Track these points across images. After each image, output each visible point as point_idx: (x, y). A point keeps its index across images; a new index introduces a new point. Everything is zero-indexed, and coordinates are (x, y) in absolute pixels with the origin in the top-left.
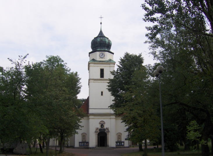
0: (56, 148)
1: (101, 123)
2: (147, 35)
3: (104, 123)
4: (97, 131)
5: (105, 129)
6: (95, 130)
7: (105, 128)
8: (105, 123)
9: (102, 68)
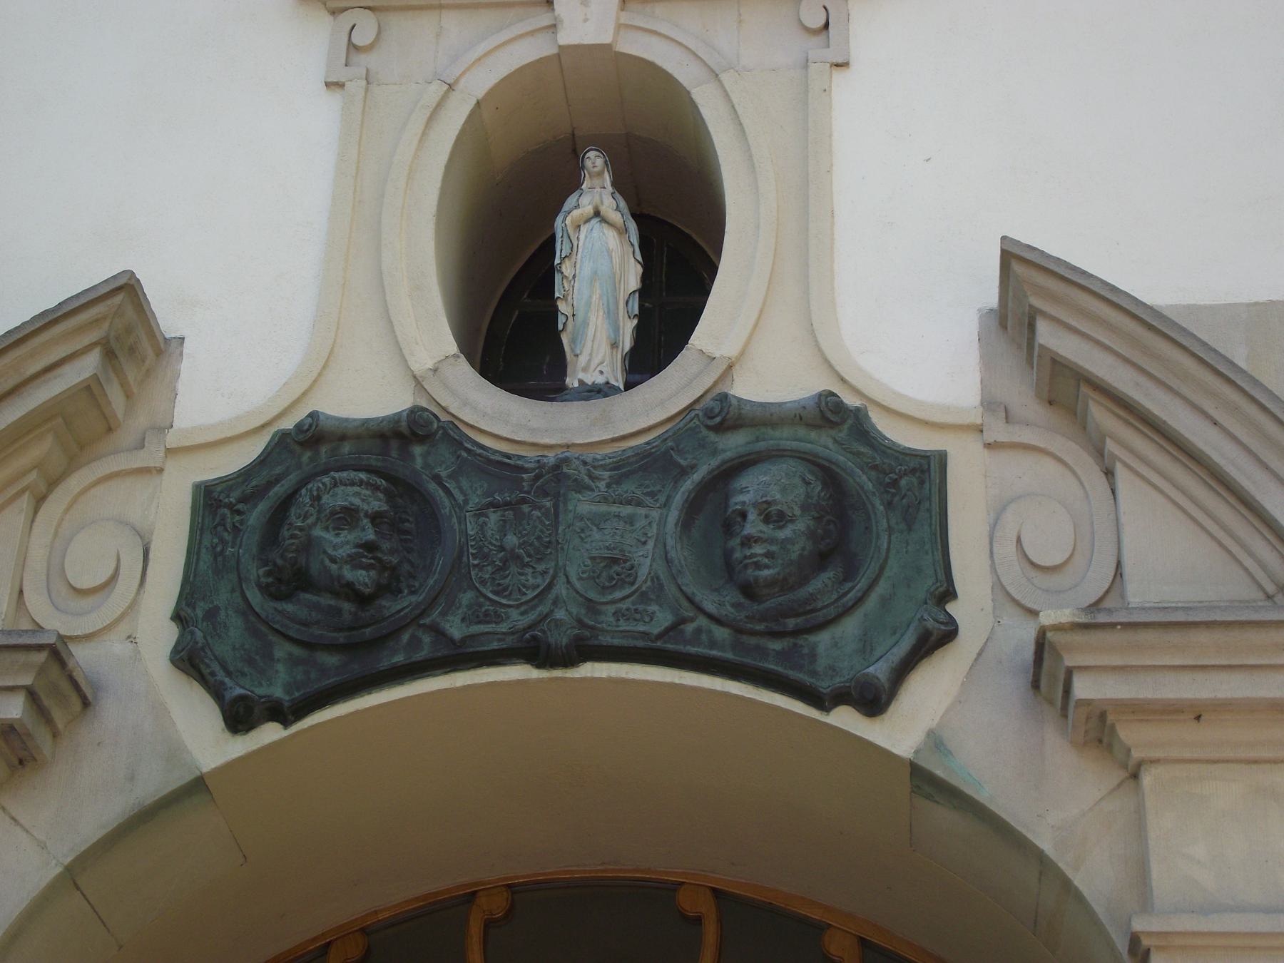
9: (580, 369)
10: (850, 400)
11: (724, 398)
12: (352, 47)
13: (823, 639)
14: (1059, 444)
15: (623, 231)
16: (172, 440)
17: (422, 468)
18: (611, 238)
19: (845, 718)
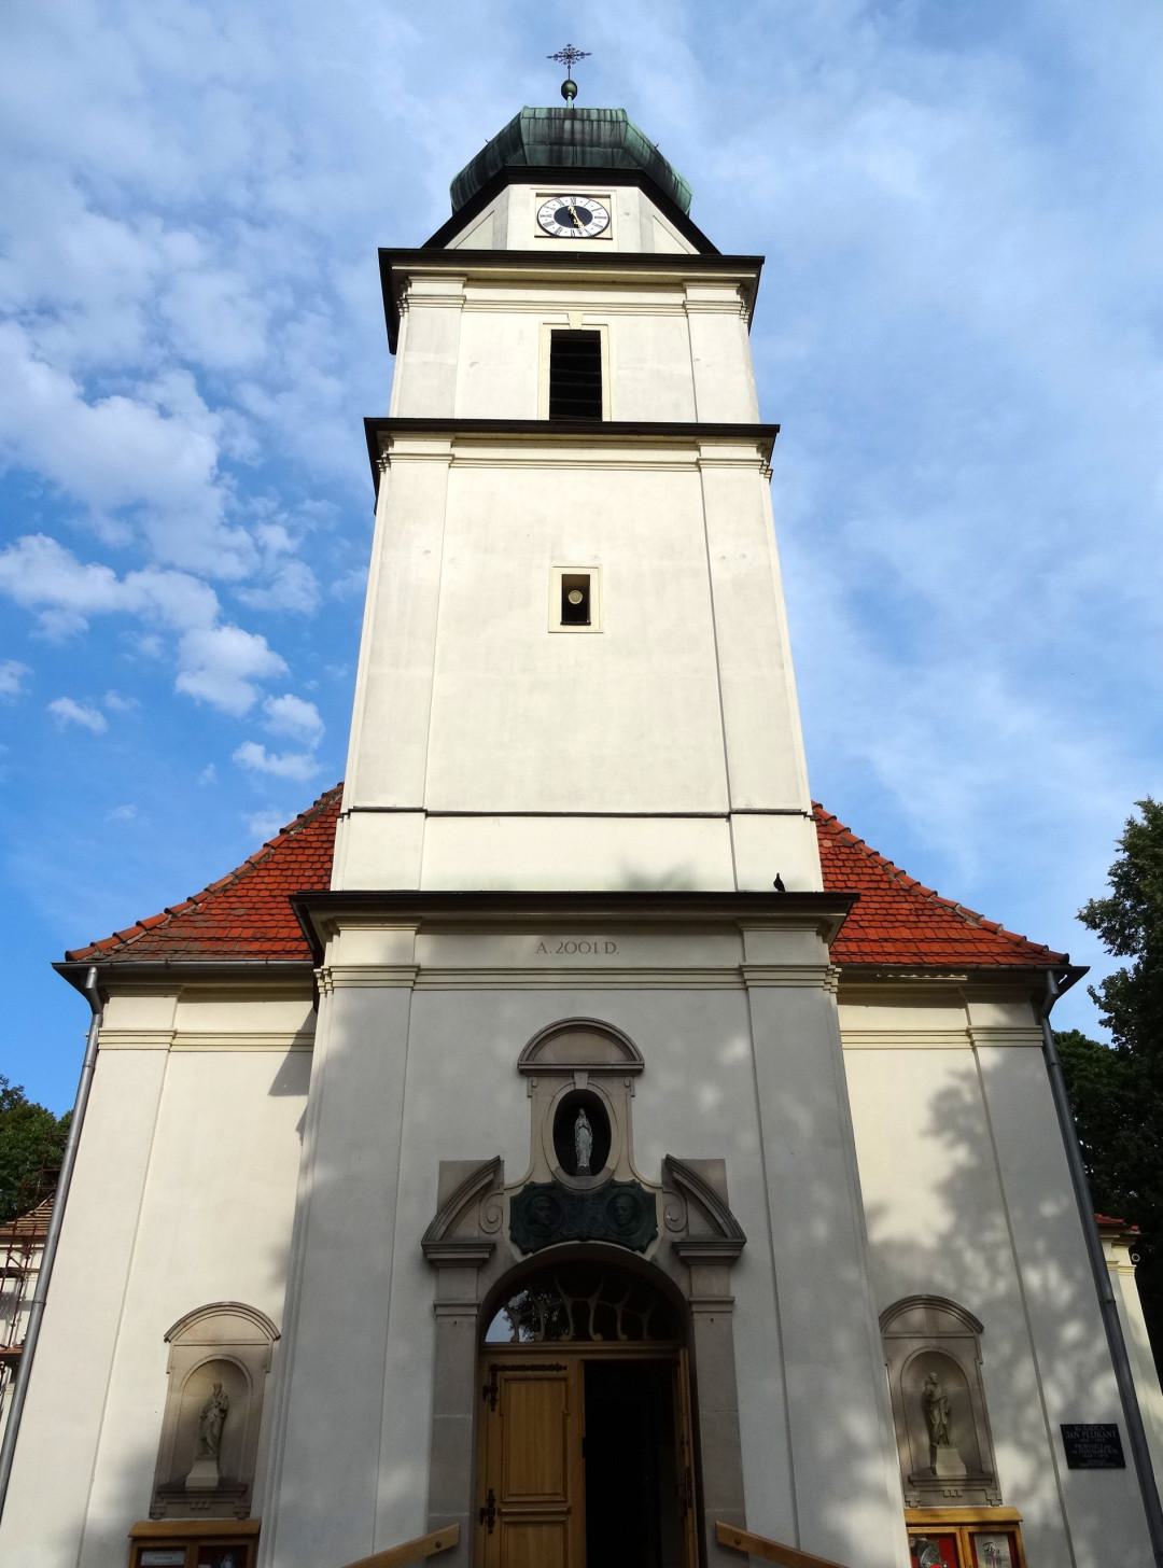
0: (35, 1271)
1: (550, 1055)
2: (1100, 937)
3: (612, 1056)
4: (469, 1229)
5: (633, 1204)
6: (419, 1213)
7: (650, 1174)
8: (632, 1069)
9: (577, 321)
10: (637, 1181)
11: (613, 1180)
12: (533, 1087)
13: (633, 1237)
14: (676, 1193)
15: (588, 1129)
16: (505, 1187)
17: (524, 1253)
18: (586, 1131)
19: (638, 1253)
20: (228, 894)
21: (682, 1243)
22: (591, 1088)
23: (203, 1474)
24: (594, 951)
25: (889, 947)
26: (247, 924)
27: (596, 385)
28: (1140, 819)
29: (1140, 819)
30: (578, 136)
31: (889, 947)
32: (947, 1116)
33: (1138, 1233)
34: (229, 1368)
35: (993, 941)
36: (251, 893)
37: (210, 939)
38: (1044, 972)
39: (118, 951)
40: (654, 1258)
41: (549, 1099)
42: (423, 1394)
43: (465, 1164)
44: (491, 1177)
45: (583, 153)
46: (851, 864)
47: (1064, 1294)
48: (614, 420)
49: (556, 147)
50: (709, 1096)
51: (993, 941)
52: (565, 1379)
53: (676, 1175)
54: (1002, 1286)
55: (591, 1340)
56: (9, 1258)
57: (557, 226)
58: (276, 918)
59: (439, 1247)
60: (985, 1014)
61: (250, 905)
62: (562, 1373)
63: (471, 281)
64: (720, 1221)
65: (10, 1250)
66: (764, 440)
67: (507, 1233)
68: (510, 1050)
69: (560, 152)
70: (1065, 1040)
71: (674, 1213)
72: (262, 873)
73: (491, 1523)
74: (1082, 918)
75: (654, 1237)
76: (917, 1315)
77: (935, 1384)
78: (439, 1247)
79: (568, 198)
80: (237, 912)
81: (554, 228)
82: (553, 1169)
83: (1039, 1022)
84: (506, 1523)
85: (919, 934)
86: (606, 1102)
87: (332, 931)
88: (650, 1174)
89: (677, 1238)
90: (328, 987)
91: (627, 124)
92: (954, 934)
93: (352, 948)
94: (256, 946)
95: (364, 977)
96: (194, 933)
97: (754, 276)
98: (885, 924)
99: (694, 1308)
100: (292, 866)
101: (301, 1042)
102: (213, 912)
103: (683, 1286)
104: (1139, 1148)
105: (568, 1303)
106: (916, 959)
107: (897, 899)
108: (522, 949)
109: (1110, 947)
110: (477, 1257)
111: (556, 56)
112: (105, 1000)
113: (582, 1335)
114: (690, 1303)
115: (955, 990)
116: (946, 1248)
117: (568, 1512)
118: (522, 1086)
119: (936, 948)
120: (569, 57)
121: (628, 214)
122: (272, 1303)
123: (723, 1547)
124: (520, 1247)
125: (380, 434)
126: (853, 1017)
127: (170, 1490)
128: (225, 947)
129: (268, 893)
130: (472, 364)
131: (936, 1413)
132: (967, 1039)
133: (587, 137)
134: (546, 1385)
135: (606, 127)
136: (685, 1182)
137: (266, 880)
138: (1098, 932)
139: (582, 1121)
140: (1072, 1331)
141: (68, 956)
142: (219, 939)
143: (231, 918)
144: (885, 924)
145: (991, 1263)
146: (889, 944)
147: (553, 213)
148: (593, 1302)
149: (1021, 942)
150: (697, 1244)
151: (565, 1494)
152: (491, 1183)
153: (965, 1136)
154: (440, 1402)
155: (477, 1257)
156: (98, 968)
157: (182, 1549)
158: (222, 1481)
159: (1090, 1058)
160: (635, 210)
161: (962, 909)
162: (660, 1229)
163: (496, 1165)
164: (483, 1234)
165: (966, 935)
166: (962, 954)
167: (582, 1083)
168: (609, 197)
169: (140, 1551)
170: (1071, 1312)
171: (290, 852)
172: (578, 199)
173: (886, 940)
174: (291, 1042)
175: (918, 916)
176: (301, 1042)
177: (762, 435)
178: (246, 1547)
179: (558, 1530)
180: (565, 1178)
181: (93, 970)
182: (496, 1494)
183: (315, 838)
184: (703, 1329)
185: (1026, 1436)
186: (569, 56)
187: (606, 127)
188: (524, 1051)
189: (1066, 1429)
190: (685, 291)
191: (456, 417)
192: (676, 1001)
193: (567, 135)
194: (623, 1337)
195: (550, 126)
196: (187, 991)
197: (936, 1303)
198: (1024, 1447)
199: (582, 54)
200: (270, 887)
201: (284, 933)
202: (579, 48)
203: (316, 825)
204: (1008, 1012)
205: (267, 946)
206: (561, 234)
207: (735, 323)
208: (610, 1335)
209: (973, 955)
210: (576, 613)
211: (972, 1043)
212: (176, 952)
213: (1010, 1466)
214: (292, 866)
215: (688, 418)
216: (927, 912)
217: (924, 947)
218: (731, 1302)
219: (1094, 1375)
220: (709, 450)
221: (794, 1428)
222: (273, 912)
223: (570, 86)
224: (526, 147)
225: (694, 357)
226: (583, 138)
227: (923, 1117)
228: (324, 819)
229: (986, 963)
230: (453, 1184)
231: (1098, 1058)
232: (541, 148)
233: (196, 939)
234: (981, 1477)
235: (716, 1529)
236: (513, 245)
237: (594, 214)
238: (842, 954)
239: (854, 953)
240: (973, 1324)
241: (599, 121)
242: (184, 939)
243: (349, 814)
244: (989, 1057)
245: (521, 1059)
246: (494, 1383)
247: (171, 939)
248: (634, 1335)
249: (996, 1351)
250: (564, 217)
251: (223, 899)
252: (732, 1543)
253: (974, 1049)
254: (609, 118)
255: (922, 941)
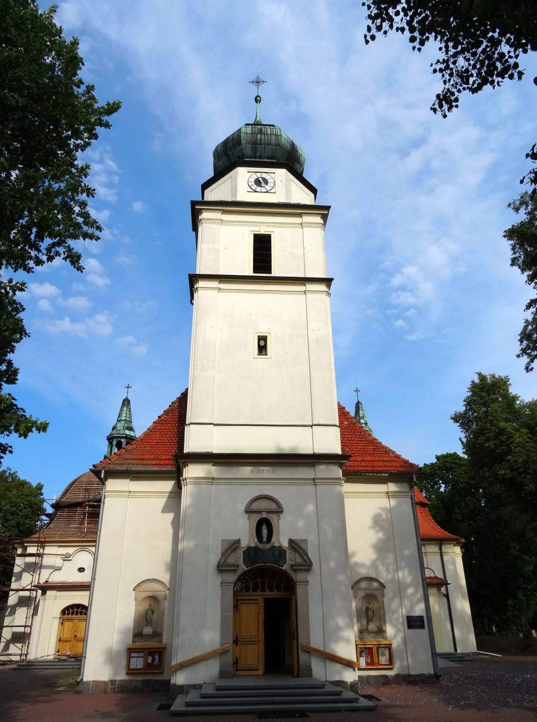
1: (256, 506)
2: (459, 426)
3: (274, 507)
4: (231, 560)
5: (280, 553)
6: (215, 557)
7: (285, 544)
8: (279, 511)
9: (263, 231)
17: (247, 567)
19: (281, 567)
20: (143, 441)
21: (295, 565)
22: (267, 517)
23: (148, 630)
24: (266, 472)
25: (363, 464)
26: (151, 453)
27: (268, 252)
28: (477, 381)
29: (477, 381)
30: (263, 141)
31: (363, 464)
32: (377, 522)
33: (464, 541)
34: (154, 599)
35: (398, 461)
36: (151, 441)
37: (139, 459)
38: (412, 474)
39: (109, 464)
40: (286, 569)
41: (254, 520)
42: (218, 609)
43: (229, 541)
44: (237, 545)
45: (265, 148)
46: (353, 431)
47: (409, 579)
48: (276, 276)
49: (254, 146)
50: (301, 523)
51: (398, 461)
52: (259, 603)
53: (293, 544)
54: (390, 577)
55: (266, 591)
56: (38, 550)
57: (255, 186)
58: (160, 451)
59: (222, 566)
60: (392, 487)
61: (151, 446)
62: (258, 601)
63: (224, 212)
64: (306, 558)
65: (38, 546)
66: (328, 283)
67: (242, 561)
68: (242, 507)
69: (256, 147)
70: (450, 456)
71: (292, 555)
72: (154, 433)
73: (237, 644)
74: (452, 418)
75: (286, 562)
76: (363, 584)
77: (369, 604)
78: (222, 566)
79: (259, 174)
80: (146, 449)
81: (254, 187)
82: (256, 542)
83: (410, 489)
84: (242, 644)
85: (374, 458)
86: (272, 521)
87: (186, 465)
88: (285, 544)
89: (293, 563)
90: (185, 484)
91: (281, 136)
92: (385, 459)
93: (192, 471)
94: (155, 462)
95: (197, 481)
96: (134, 457)
97: (327, 212)
98: (363, 455)
99: (297, 584)
100: (164, 430)
101: (171, 495)
102: (139, 448)
103: (294, 577)
104: (474, 503)
105: (259, 581)
106: (372, 469)
107: (368, 445)
108: (246, 471)
109: (463, 430)
110: (233, 569)
111: (253, 82)
112: (106, 480)
113: (263, 590)
114: (296, 582)
115: (384, 478)
116: (374, 565)
117: (259, 641)
118: (246, 516)
119: (379, 464)
120: (258, 83)
121: (281, 182)
122: (165, 578)
123: (304, 651)
124: (246, 565)
125: (194, 279)
126: (348, 487)
127: (138, 635)
128: (145, 462)
129: (156, 441)
130: (225, 248)
131: (369, 612)
132: (387, 495)
133: (266, 142)
134: (253, 605)
135: (273, 137)
136: (296, 547)
137: (155, 436)
138: (458, 424)
139: (264, 527)
140: (410, 591)
141: (94, 466)
142: (142, 459)
143: (145, 451)
144: (363, 455)
145: (387, 569)
146: (363, 463)
147: (254, 180)
148: (267, 580)
149: (406, 462)
150: (299, 565)
151: (258, 636)
152: (236, 547)
153: (382, 528)
154: (223, 610)
155: (233, 569)
156: (105, 471)
157: (143, 652)
158: (153, 632)
159: (460, 465)
160: (284, 179)
161: (389, 449)
162: (288, 560)
163: (238, 541)
164: (235, 562)
165: (389, 459)
166: (387, 466)
167: (264, 515)
168: (275, 173)
169: (130, 652)
170: (411, 585)
171: (162, 425)
172: (263, 174)
173: (363, 461)
174: (168, 495)
175: (374, 451)
176: (171, 495)
177: (328, 281)
178: (162, 651)
179: (256, 646)
180: (260, 546)
181: (103, 471)
182: (238, 636)
183: (170, 420)
184: (299, 590)
185: (394, 622)
186: (258, 82)
187: (273, 137)
188: (247, 505)
189: (408, 617)
190: (305, 286)
191: (220, 274)
192: (294, 489)
193: (259, 141)
194: (276, 591)
195: (252, 137)
196: (133, 477)
197: (370, 579)
198: (394, 625)
199: (263, 82)
200: (157, 439)
201: (164, 457)
202: (262, 79)
203: (170, 414)
204: (399, 487)
205: (159, 462)
206: (257, 190)
207: (318, 232)
208: (272, 590)
209: (390, 467)
210: (262, 349)
211: (388, 496)
212: (129, 464)
213: (390, 630)
214: (164, 430)
215: (301, 275)
216: (377, 450)
217: (375, 464)
218: (308, 582)
219: (416, 604)
220: (310, 287)
221: (324, 619)
222: (159, 449)
223: (258, 98)
224: (243, 145)
225: (305, 247)
226: (265, 143)
227: (369, 522)
228: (172, 412)
229: (393, 470)
230: (226, 546)
231: (464, 464)
232: (248, 145)
233: (135, 459)
234: (381, 631)
235: (302, 645)
236: (240, 198)
237: (269, 181)
238: (348, 466)
239: (352, 466)
240: (383, 586)
241: (271, 135)
242: (131, 459)
243: (189, 424)
244: (393, 502)
245: (246, 508)
246: (237, 604)
247: (126, 459)
248: (279, 590)
249: (388, 593)
250: (258, 182)
251: (141, 443)
252: (306, 649)
253: (389, 498)
254: (274, 134)
255: (374, 461)
